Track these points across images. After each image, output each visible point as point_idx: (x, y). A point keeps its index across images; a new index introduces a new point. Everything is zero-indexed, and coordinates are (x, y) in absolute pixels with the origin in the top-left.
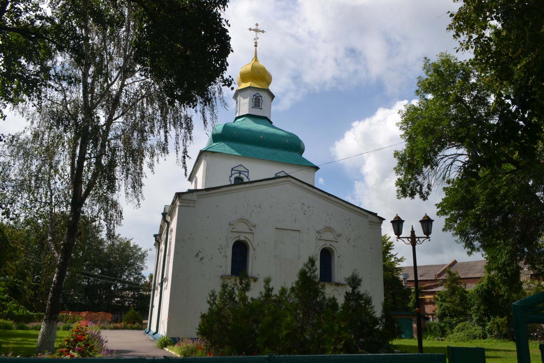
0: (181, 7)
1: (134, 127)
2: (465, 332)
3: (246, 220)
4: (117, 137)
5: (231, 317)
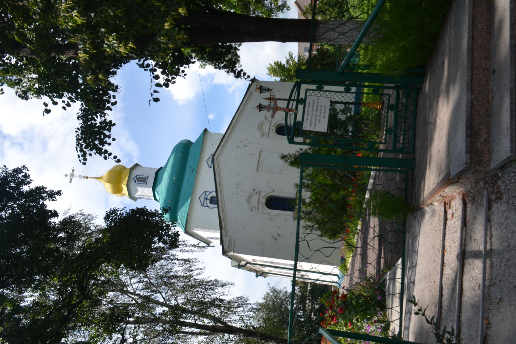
3: (249, 196)
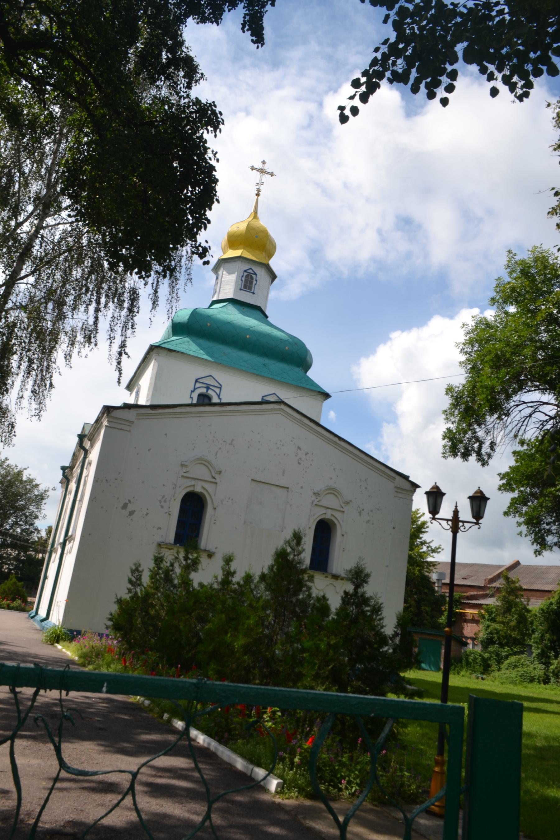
0: (147, 120)
1: (50, 294)
2: (518, 671)
3: (208, 462)
4: (16, 307)
5: (165, 608)
